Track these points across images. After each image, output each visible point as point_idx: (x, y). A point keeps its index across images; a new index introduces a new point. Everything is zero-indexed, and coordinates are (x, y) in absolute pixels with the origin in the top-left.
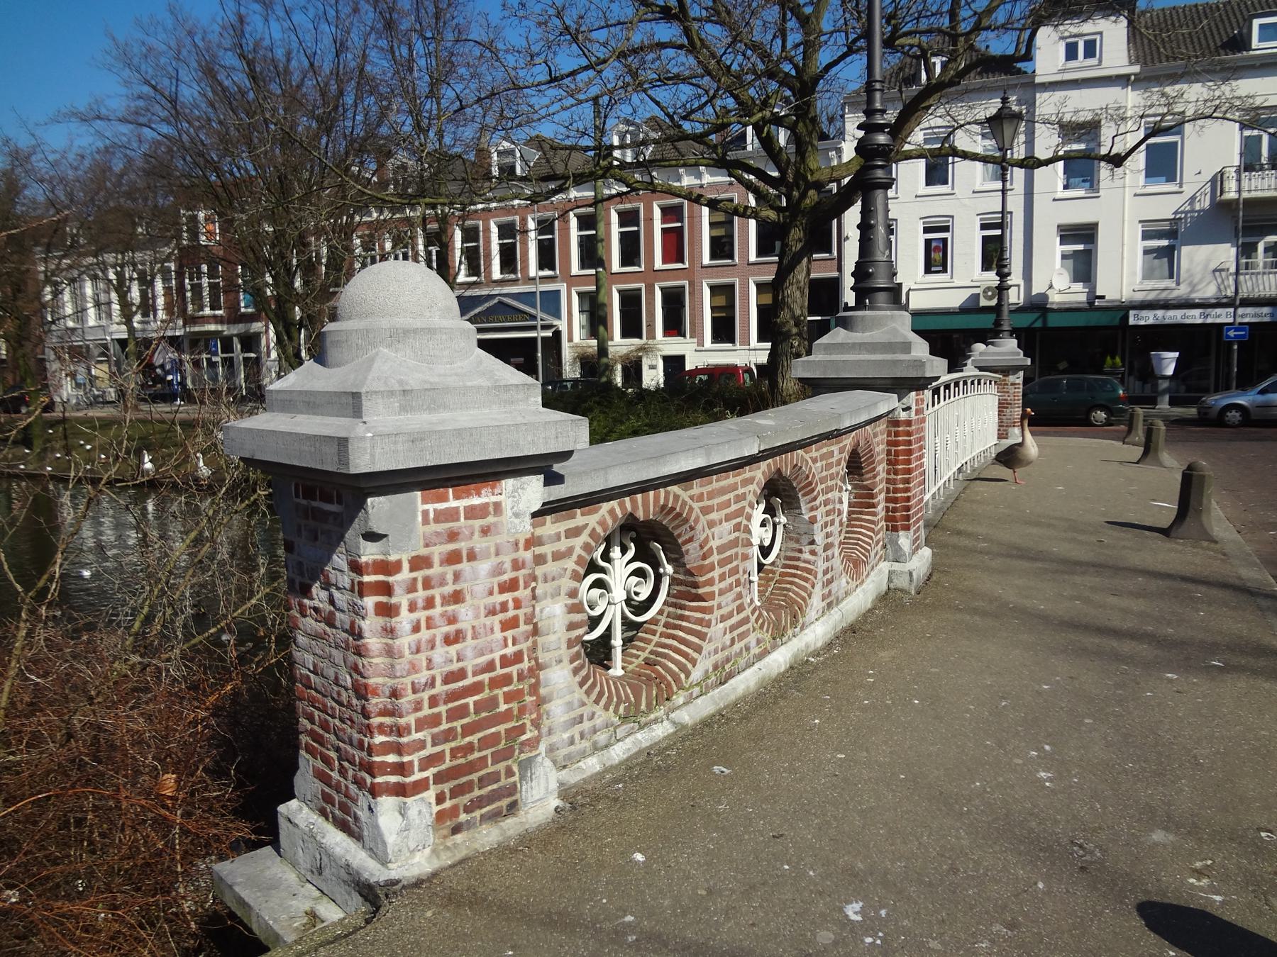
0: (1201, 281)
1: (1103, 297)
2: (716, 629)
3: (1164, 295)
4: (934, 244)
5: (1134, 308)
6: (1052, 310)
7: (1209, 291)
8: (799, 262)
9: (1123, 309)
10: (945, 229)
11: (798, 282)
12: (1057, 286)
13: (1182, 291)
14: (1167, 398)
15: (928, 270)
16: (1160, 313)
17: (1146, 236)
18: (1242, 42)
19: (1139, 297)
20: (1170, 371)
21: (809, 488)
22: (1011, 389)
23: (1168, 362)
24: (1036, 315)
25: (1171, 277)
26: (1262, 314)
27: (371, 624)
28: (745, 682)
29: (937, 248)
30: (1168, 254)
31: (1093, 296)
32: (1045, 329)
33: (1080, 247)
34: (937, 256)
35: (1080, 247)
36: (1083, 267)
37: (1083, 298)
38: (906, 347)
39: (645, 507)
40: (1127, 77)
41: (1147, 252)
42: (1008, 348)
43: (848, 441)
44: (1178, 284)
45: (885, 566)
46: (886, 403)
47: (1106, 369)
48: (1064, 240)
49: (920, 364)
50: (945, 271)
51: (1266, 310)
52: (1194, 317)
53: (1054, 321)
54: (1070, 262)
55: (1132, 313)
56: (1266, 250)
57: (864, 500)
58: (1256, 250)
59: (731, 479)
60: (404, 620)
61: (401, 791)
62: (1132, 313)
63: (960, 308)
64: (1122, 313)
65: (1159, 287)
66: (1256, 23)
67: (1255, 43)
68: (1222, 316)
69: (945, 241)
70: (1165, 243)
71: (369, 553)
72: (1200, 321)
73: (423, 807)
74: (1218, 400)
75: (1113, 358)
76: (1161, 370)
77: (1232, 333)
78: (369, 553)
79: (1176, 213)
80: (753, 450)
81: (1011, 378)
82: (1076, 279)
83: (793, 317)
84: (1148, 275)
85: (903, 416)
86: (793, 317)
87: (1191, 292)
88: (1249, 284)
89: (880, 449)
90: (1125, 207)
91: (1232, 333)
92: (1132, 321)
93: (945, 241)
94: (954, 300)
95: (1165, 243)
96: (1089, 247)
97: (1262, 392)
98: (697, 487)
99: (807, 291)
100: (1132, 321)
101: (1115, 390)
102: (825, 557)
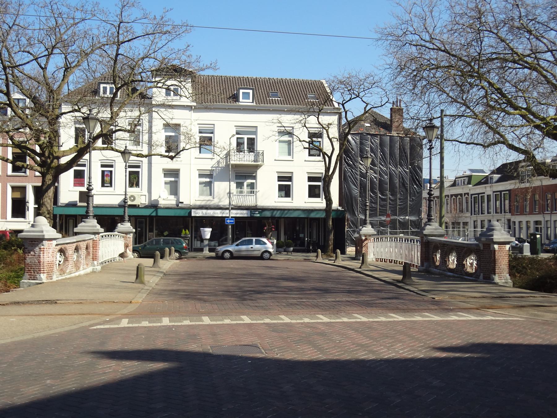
0: (223, 198)
1: (182, 203)
2: (70, 266)
3: (208, 203)
4: (106, 173)
5: (194, 208)
6: (161, 208)
7: (225, 202)
8: (50, 188)
9: (190, 209)
10: (111, 166)
11: (49, 196)
12: (162, 197)
13: (215, 202)
14: (207, 248)
15: (103, 185)
16: (204, 211)
17: (201, 176)
18: (235, 98)
19: (198, 203)
20: (208, 236)
21: (81, 249)
22: (128, 239)
23: (207, 232)
24: (153, 210)
25: (211, 195)
26: (244, 214)
27: (42, 255)
28: (73, 275)
29: (107, 175)
30: (209, 184)
31: (179, 202)
32: (157, 216)
33: (173, 179)
34: (107, 179)
35: (173, 179)
36: (174, 189)
37: (174, 202)
38: (96, 226)
39: (63, 246)
40: (191, 107)
41: (201, 183)
42: (127, 226)
43: (86, 242)
44: (214, 198)
45: (92, 267)
46: (92, 236)
47: (182, 235)
48: (166, 175)
49: (98, 230)
50: (111, 186)
51: (245, 212)
52: (218, 213)
53: (161, 213)
54: (168, 186)
55: (193, 211)
56: (247, 186)
57: (88, 254)
58: (243, 186)
59: (71, 245)
60: (45, 254)
61: (44, 273)
62: (193, 211)
63: (119, 205)
64: (189, 211)
65: (204, 200)
66: (241, 91)
67: (241, 100)
68: (226, 213)
69: (111, 172)
70: (208, 180)
71: (42, 247)
72: (220, 215)
73: (45, 274)
74: (221, 249)
75: (185, 230)
76: (205, 236)
77: (228, 221)
78: (42, 247)
79: (212, 167)
80: (75, 241)
81: (128, 236)
82: (171, 194)
83: (48, 210)
84: (201, 194)
85: (95, 239)
86: (48, 210)
87: (219, 202)
88: (242, 200)
89: (91, 245)
90: (192, 164)
91: (228, 221)
92: (193, 215)
93: (111, 172)
94: (116, 200)
95: (208, 180)
96: (176, 179)
97: (237, 245)
98: (68, 245)
99: (53, 200)
100: (193, 215)
101: (182, 244)
102: (83, 261)
